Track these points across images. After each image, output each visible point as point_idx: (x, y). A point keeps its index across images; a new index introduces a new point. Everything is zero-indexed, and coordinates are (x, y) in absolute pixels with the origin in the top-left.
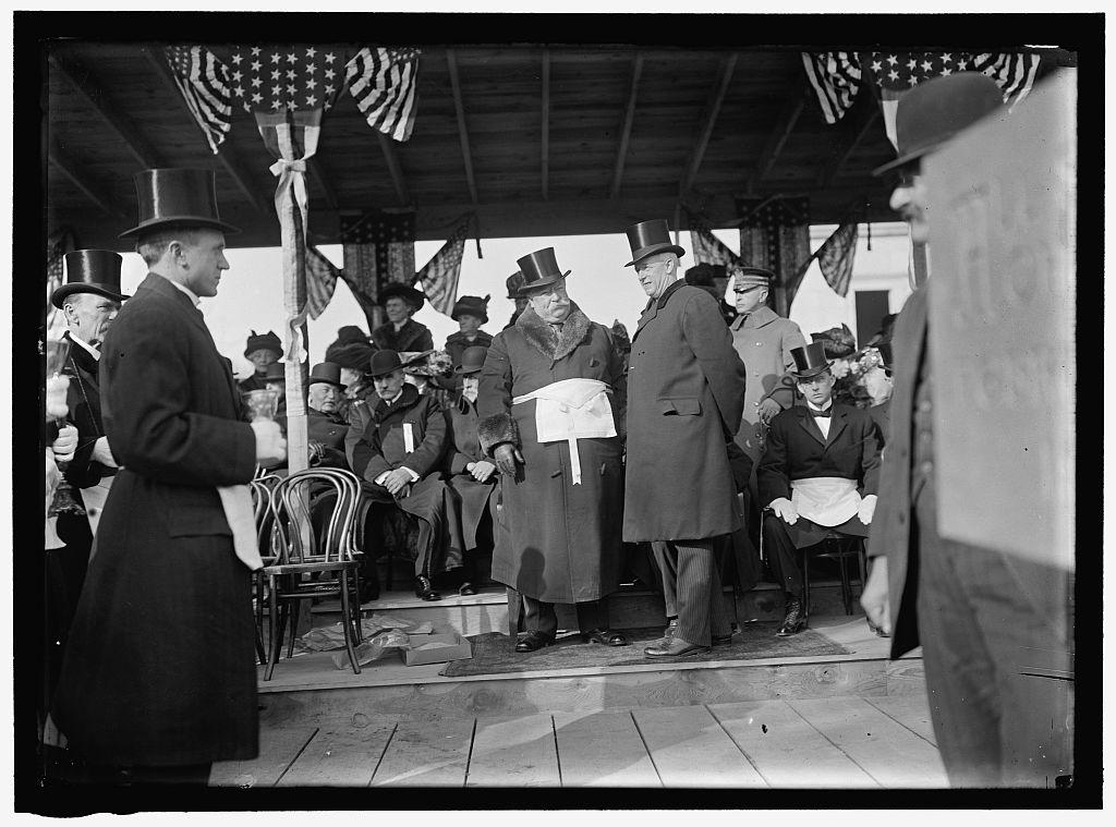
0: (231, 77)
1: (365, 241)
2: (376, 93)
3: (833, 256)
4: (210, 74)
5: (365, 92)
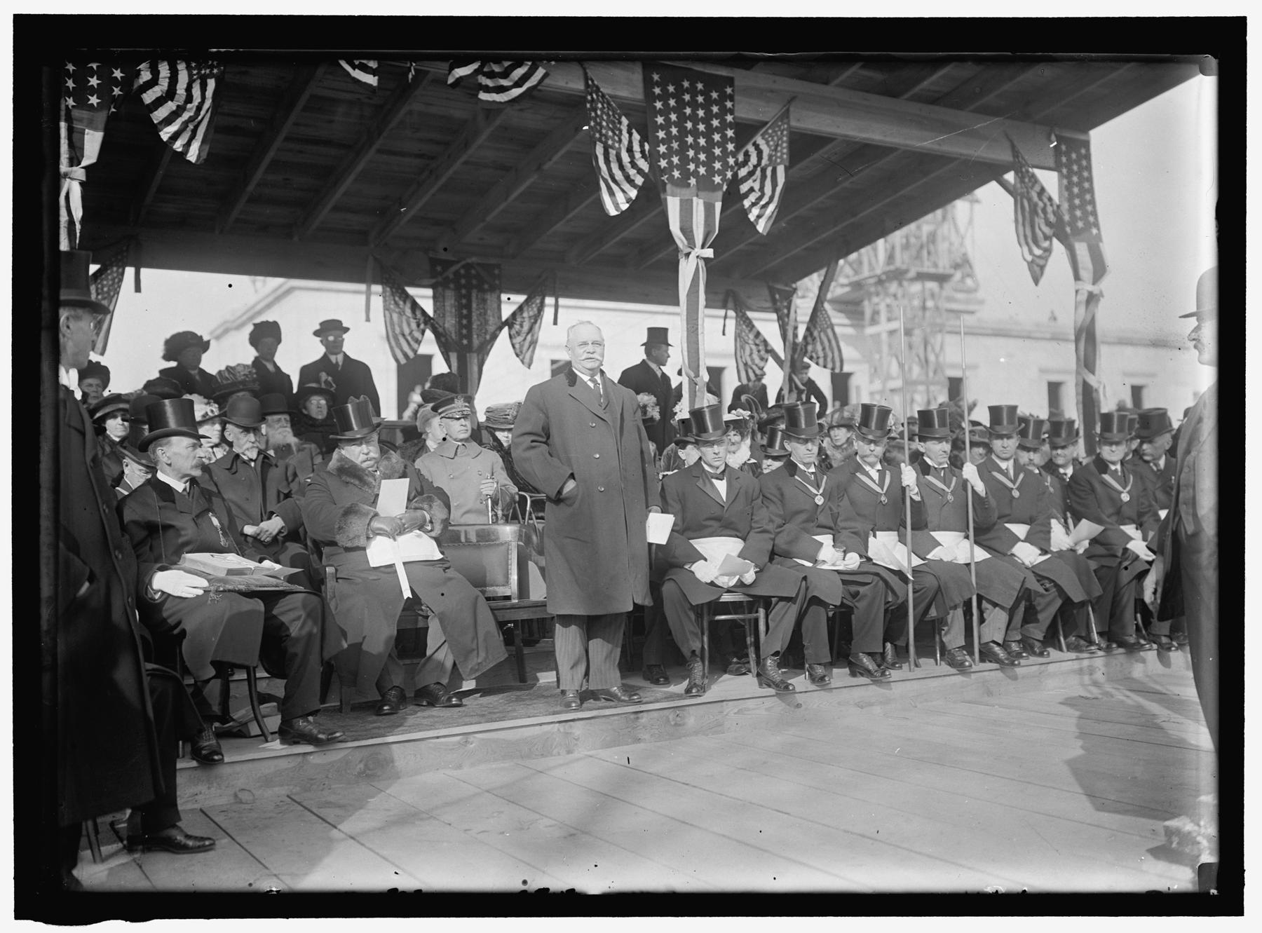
2: (171, 106)
3: (521, 326)
5: (159, 102)
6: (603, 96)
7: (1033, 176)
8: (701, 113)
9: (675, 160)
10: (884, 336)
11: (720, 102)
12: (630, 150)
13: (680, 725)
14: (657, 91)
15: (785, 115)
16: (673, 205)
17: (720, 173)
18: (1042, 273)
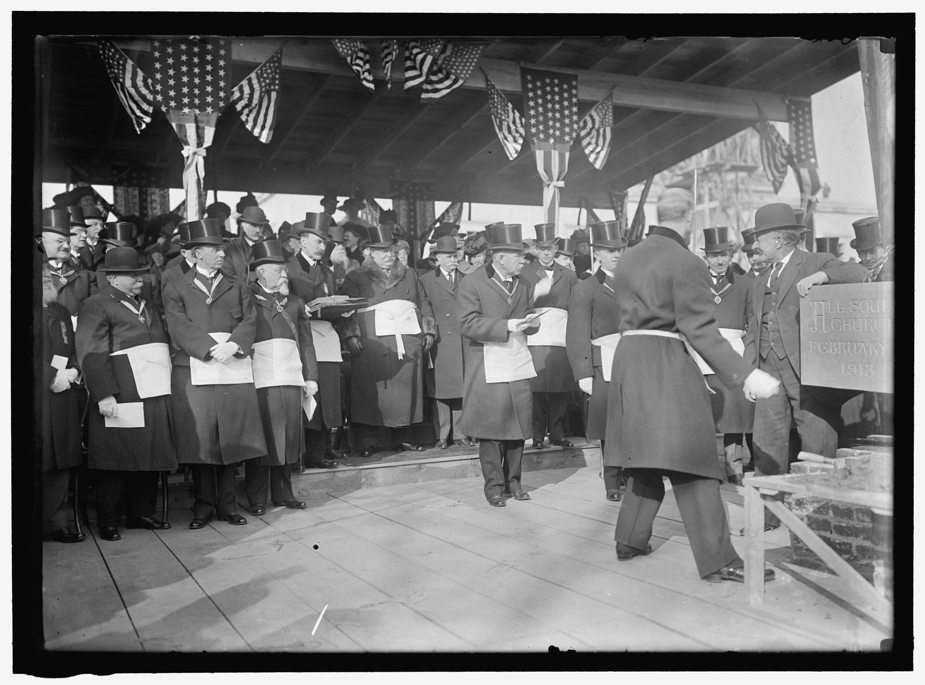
0: (154, 87)
1: (130, 185)
4: (140, 83)
6: (497, 91)
7: (773, 127)
8: (557, 98)
9: (541, 127)
10: (707, 212)
11: (569, 91)
12: (514, 122)
13: (540, 463)
14: (530, 86)
15: (610, 97)
16: (540, 156)
17: (568, 134)
18: (780, 187)
